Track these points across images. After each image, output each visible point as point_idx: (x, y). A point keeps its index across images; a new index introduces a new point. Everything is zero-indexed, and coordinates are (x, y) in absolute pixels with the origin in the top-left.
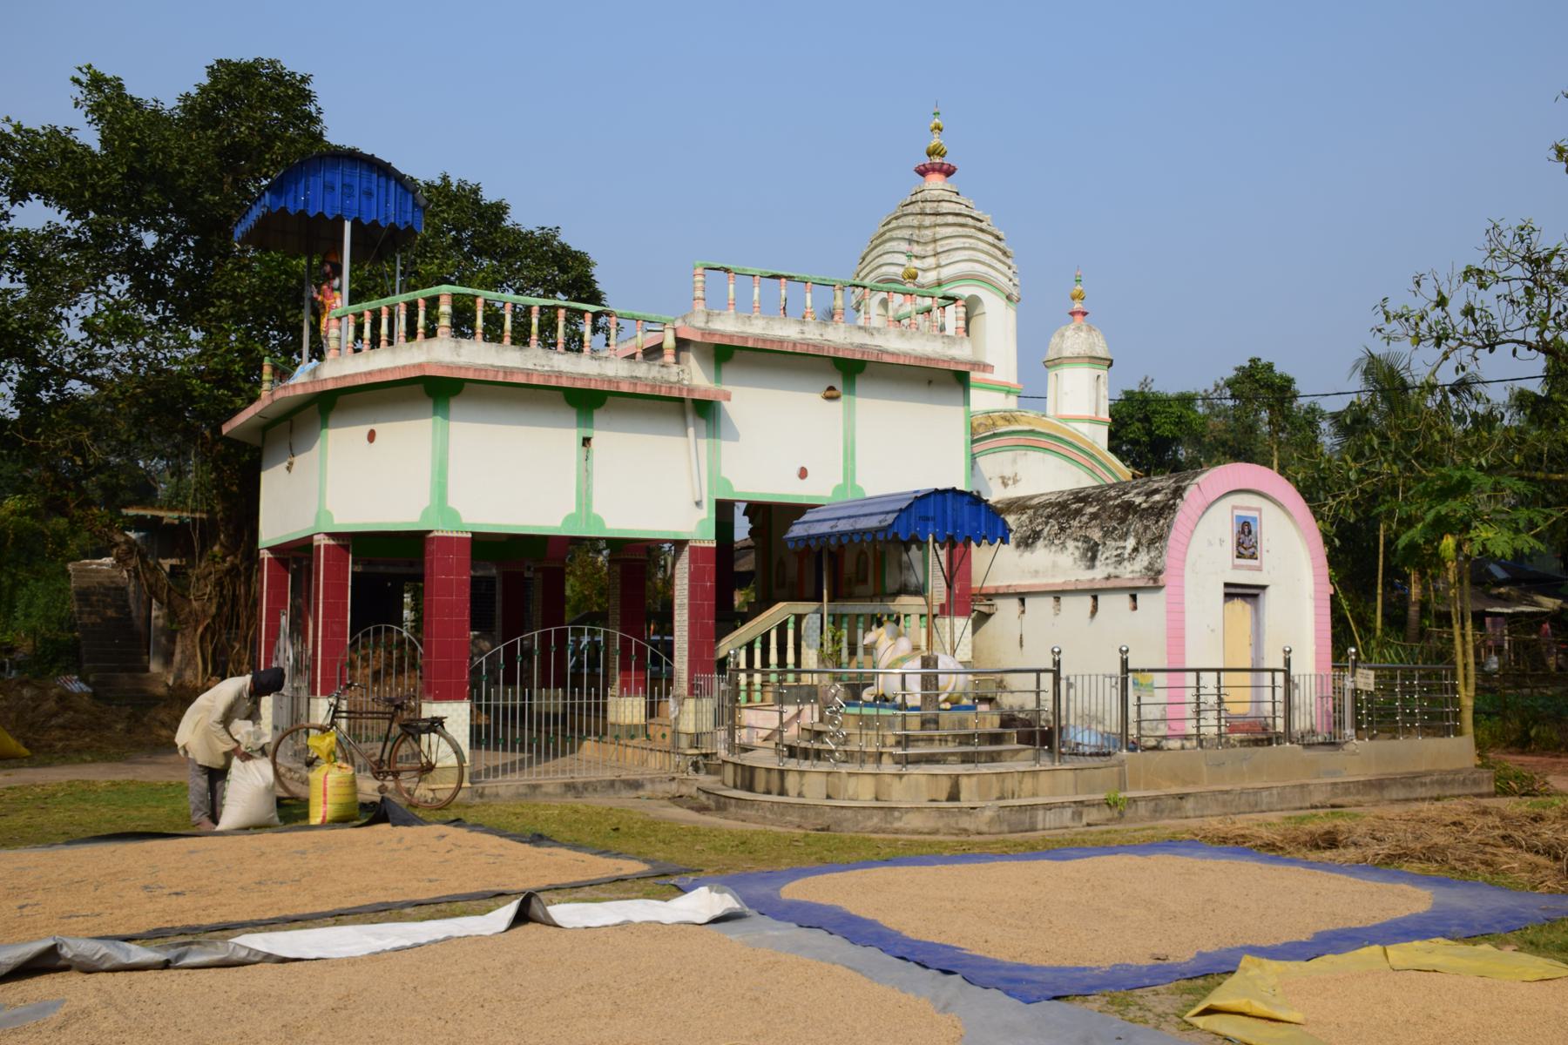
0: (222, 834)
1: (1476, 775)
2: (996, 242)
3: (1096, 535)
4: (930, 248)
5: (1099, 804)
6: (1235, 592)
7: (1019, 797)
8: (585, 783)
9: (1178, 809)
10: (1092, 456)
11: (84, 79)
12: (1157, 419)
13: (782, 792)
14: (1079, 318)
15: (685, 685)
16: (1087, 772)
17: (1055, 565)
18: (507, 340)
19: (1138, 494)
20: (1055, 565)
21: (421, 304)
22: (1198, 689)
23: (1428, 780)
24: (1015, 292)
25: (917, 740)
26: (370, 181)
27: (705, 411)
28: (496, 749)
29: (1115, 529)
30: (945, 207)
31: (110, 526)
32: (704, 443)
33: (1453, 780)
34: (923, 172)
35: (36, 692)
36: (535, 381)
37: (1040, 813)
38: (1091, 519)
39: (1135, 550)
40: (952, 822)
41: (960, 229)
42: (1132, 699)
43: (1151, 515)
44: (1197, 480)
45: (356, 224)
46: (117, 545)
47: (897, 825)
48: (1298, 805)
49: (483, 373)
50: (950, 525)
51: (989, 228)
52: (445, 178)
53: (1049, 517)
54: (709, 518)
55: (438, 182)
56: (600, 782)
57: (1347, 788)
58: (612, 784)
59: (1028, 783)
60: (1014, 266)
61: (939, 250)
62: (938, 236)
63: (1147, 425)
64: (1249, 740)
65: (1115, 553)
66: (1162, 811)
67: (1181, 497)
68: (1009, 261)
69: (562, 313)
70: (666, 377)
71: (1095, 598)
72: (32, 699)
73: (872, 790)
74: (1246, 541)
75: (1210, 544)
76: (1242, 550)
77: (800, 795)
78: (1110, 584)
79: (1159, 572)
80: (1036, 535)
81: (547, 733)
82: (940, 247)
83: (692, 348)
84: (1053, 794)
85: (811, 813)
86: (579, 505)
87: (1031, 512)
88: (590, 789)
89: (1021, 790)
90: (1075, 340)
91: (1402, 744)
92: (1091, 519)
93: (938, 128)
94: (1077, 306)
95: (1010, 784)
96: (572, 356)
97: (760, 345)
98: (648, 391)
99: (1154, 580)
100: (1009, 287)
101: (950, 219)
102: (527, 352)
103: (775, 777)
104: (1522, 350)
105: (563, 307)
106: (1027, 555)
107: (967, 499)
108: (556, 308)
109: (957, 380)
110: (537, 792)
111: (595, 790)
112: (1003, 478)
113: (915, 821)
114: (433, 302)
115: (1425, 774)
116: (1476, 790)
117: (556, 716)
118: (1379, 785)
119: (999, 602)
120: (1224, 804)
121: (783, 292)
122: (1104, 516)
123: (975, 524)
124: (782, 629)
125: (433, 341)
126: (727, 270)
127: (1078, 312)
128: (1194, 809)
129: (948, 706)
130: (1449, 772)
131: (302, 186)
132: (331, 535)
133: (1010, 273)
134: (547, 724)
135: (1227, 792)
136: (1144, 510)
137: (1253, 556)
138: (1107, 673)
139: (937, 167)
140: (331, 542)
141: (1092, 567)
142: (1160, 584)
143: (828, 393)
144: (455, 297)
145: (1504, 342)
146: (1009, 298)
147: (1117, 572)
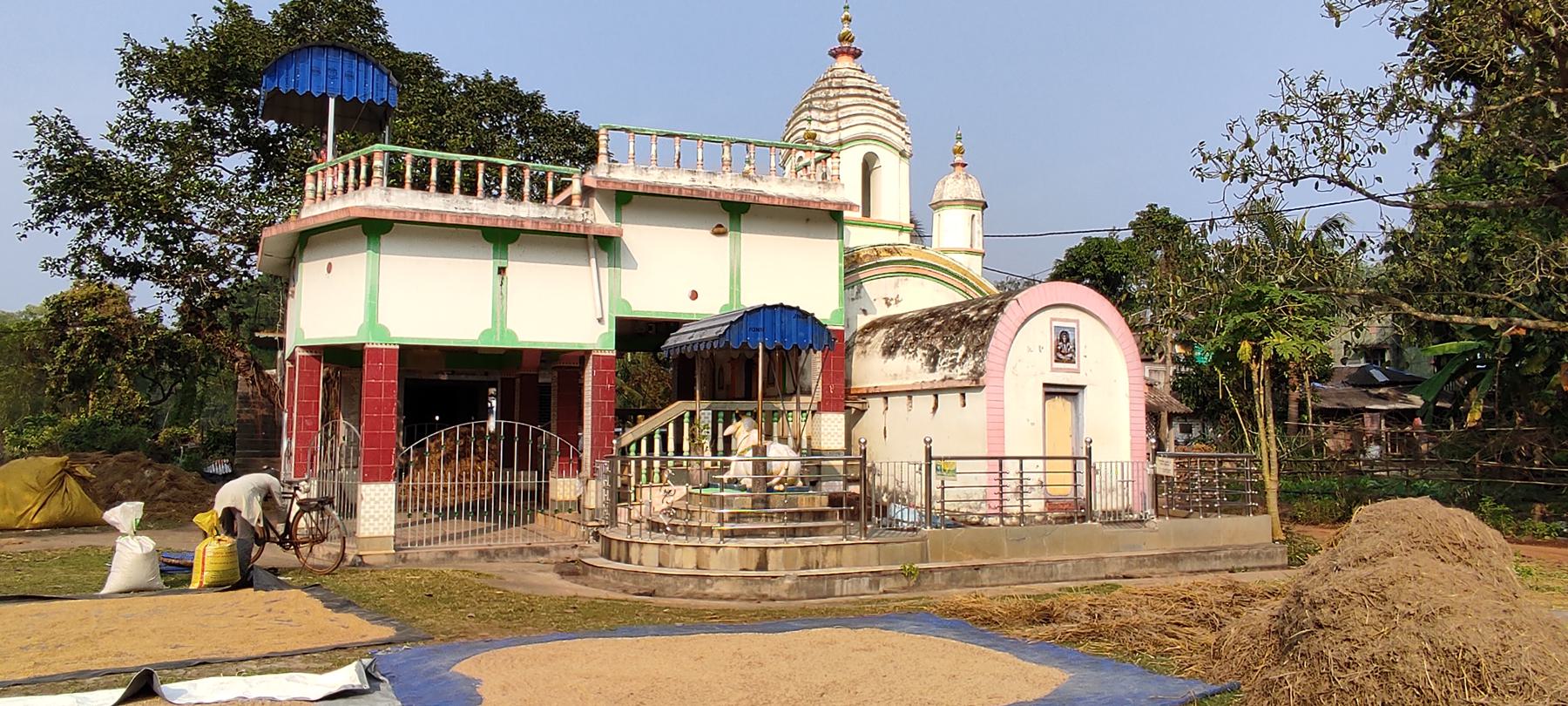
0: (103, 597)
1: (1270, 550)
2: (891, 109)
3: (938, 344)
4: (833, 115)
5: (895, 574)
6: (1052, 391)
7: (823, 567)
8: (497, 550)
9: (975, 578)
10: (965, 281)
11: (223, 7)
12: (1108, 258)
13: (628, 561)
14: (959, 168)
15: (589, 469)
16: (890, 545)
17: (908, 369)
18: (408, 186)
19: (973, 309)
20: (908, 369)
21: (363, 158)
22: (1001, 474)
23: (1222, 554)
24: (908, 149)
25: (747, 517)
26: (351, 66)
27: (607, 245)
28: (467, 518)
29: (952, 338)
30: (849, 82)
31: (232, 346)
32: (605, 271)
33: (1247, 553)
34: (835, 54)
35: (155, 472)
36: (448, 221)
37: (838, 582)
38: (936, 331)
39: (965, 356)
40: (755, 588)
41: (859, 99)
42: (936, 483)
43: (978, 326)
44: (1016, 297)
45: (339, 100)
46: (237, 360)
47: (709, 591)
48: (1093, 576)
49: (384, 213)
50: (778, 337)
51: (886, 98)
52: (487, 74)
53: (908, 330)
54: (610, 332)
55: (482, 78)
56: (511, 549)
57: (1141, 561)
58: (521, 550)
59: (832, 555)
60: (907, 128)
61: (840, 116)
62: (840, 105)
63: (1101, 263)
64: (1064, 518)
65: (950, 359)
66: (958, 581)
67: (1002, 311)
68: (902, 124)
69: (481, 166)
70: (572, 217)
71: (936, 396)
72: (151, 478)
73: (694, 559)
74: (1064, 347)
75: (1030, 350)
76: (1060, 355)
77: (640, 563)
78: (945, 385)
79: (981, 374)
80: (897, 345)
81: (525, 508)
82: (840, 114)
83: (596, 194)
84: (857, 565)
85: (641, 579)
86: (494, 322)
87: (897, 326)
88: (501, 555)
89: (825, 561)
90: (954, 186)
91: (1199, 522)
92: (936, 331)
93: (848, 19)
94: (958, 159)
95: (814, 555)
96: (489, 202)
97: (649, 191)
98: (549, 228)
99: (976, 383)
100: (902, 146)
101: (852, 91)
102: (450, 198)
103: (623, 546)
104: (1323, 183)
105: (482, 162)
106: (890, 360)
107: (795, 312)
108: (477, 162)
109: (831, 219)
110: (454, 557)
111: (506, 555)
112: (886, 299)
113: (724, 588)
114: (370, 158)
115: (1220, 549)
116: (1270, 563)
117: (532, 492)
118: (1174, 558)
119: (870, 400)
120: (1020, 574)
121: (677, 148)
122: (946, 328)
123: (801, 334)
124: (679, 422)
125: (369, 190)
126: (627, 131)
127: (958, 164)
128: (990, 579)
129: (781, 487)
130: (1243, 547)
131: (292, 71)
132: (304, 348)
133: (903, 134)
134: (518, 499)
135: (1022, 564)
136: (974, 322)
137: (1071, 361)
138: (911, 460)
139: (845, 50)
140: (306, 354)
141: (933, 371)
142: (981, 384)
143: (716, 230)
144: (416, 159)
145: (1306, 177)
146: (902, 154)
147: (951, 375)
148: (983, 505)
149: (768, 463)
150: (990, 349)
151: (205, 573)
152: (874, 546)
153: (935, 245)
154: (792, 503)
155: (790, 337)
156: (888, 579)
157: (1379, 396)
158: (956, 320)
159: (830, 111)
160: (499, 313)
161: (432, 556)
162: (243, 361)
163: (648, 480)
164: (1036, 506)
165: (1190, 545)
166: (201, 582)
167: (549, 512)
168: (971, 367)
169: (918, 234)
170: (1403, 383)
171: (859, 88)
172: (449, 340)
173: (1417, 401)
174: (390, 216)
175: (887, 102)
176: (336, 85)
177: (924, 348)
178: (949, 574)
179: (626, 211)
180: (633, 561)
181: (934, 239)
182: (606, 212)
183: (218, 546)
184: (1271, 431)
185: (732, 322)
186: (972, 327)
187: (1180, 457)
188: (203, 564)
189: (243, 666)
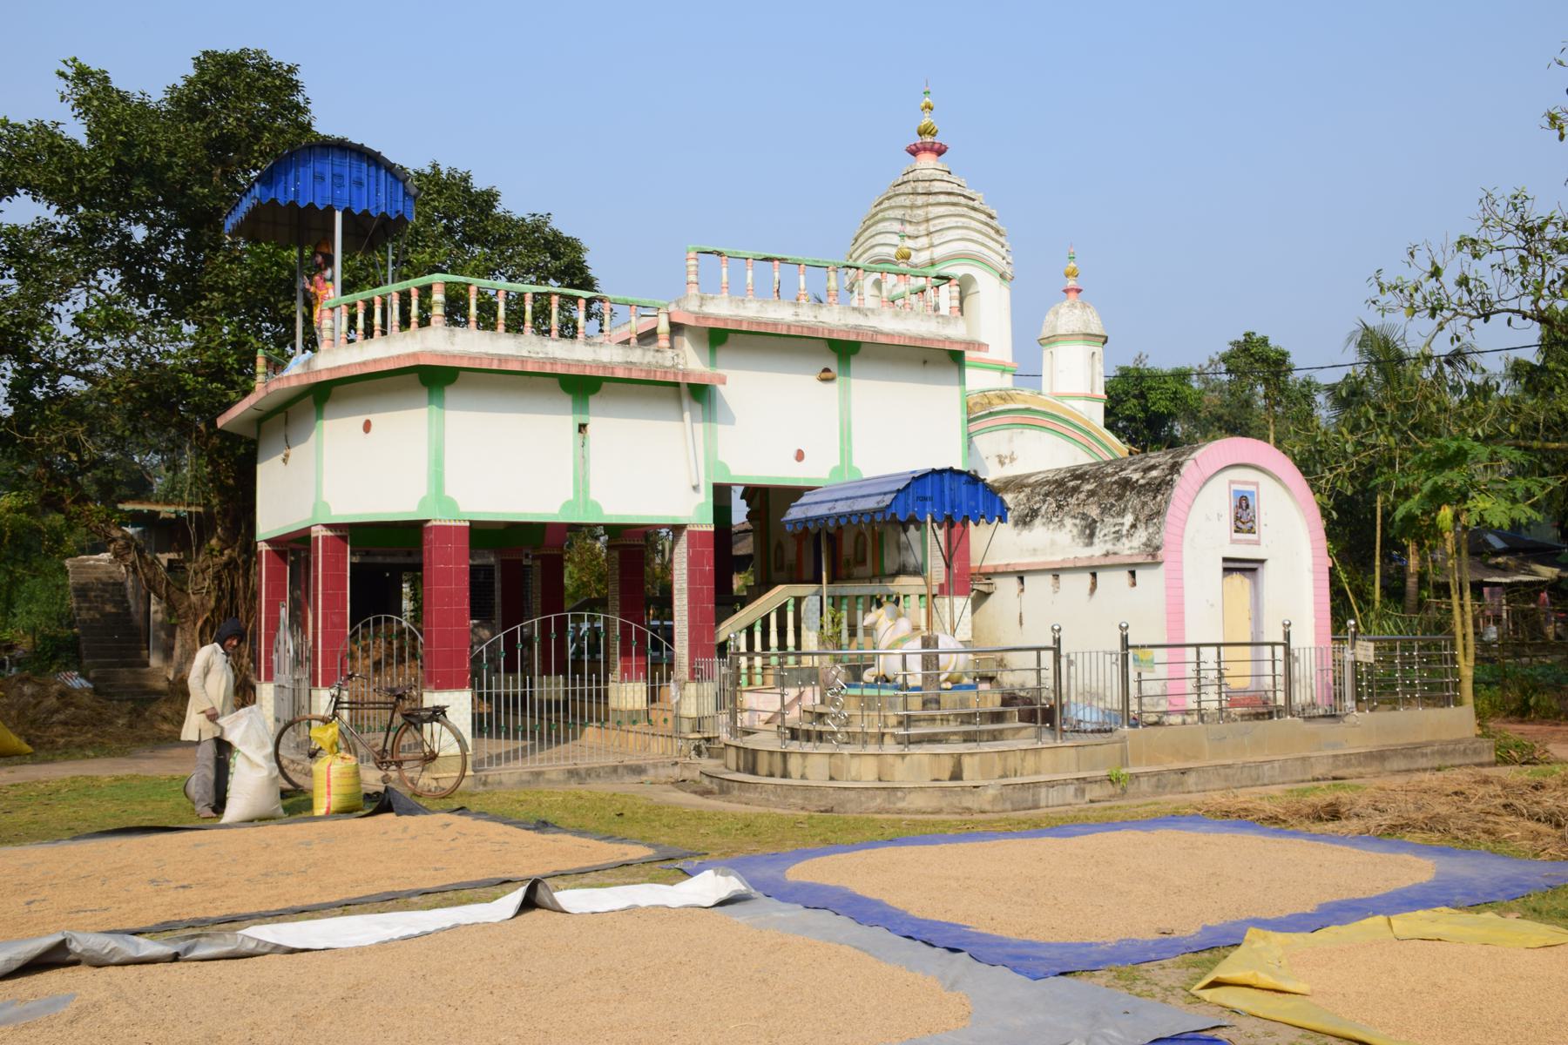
0: (227, 826)
1: (1477, 745)
2: (989, 220)
3: (1094, 512)
4: (922, 229)
7: (1022, 775)
9: (1181, 783)
11: (70, 72)
12: (1152, 396)
13: (785, 775)
14: (1072, 295)
15: (686, 670)
17: (1053, 543)
18: (501, 328)
19: (1136, 470)
20: (1053, 543)
22: (1198, 664)
23: (1428, 750)
24: (1009, 271)
25: (919, 720)
27: (700, 394)
28: (498, 737)
29: (1113, 505)
30: (937, 187)
31: (106, 522)
32: (700, 427)
34: (914, 151)
35: (37, 688)
37: (1043, 790)
39: (1134, 526)
41: (952, 208)
42: (1133, 675)
44: (1193, 455)
45: (347, 213)
47: (901, 805)
48: (1300, 778)
51: (981, 207)
52: (435, 166)
53: (1047, 495)
55: (428, 171)
57: (1348, 760)
58: (615, 769)
59: (1030, 761)
61: (932, 229)
62: (930, 216)
63: (1143, 401)
67: (1178, 472)
68: (1002, 240)
69: (555, 300)
71: (1094, 575)
72: (33, 695)
73: (875, 769)
74: (1244, 515)
75: (1208, 518)
76: (1240, 524)
77: (803, 777)
78: (1108, 561)
79: (1158, 548)
80: (1034, 513)
82: (932, 226)
83: (686, 332)
86: (576, 492)
87: (1028, 490)
88: (593, 775)
89: (1023, 767)
90: (1069, 317)
92: (1088, 497)
93: (929, 107)
94: (1071, 283)
95: (1013, 762)
98: (643, 376)
99: (1153, 555)
101: (943, 198)
102: (521, 339)
103: (778, 759)
104: (1517, 319)
105: (556, 294)
106: (1025, 533)
107: (964, 478)
108: (549, 295)
111: (598, 776)
112: (999, 457)
113: (918, 801)
114: (426, 291)
115: (1426, 745)
116: (1477, 760)
117: (557, 702)
118: (1380, 756)
119: (997, 581)
120: (1226, 778)
122: (1102, 493)
123: (972, 503)
126: (720, 254)
128: (1196, 784)
130: (1449, 742)
131: (291, 177)
132: (329, 526)
133: (1003, 252)
135: (1229, 766)
136: (1141, 486)
137: (1251, 531)
139: (928, 146)
140: (329, 533)
141: (1091, 544)
142: (1159, 559)
145: (1499, 312)
146: (1002, 276)
147: (1116, 549)
148: (1163, 702)
149: (941, 656)
150: (1168, 518)
151: (333, 797)
152: (1073, 750)
153: (1046, 389)
154: (963, 702)
155: (960, 506)
156: (1094, 786)
157: (1497, 567)
158: (1115, 482)
159: (918, 223)
160: (581, 481)
161: (515, 778)
162: (121, 542)
163: (750, 683)
164: (1211, 702)
165: (1392, 741)
166: (328, 808)
167: (610, 724)
168: (1144, 540)
169: (1029, 375)
170: (1525, 550)
171: (949, 194)
172: (526, 515)
173: (1547, 573)
174: (595, 373)
175: (983, 212)
176: (344, 194)
177: (1074, 517)
178: (1155, 779)
179: (722, 354)
180: (793, 775)
181: (1045, 380)
182: (698, 354)
183: (343, 765)
184: (1468, 608)
185: (898, 491)
186: (1139, 492)
187: (1381, 641)
188: (329, 786)
189: (587, 879)
